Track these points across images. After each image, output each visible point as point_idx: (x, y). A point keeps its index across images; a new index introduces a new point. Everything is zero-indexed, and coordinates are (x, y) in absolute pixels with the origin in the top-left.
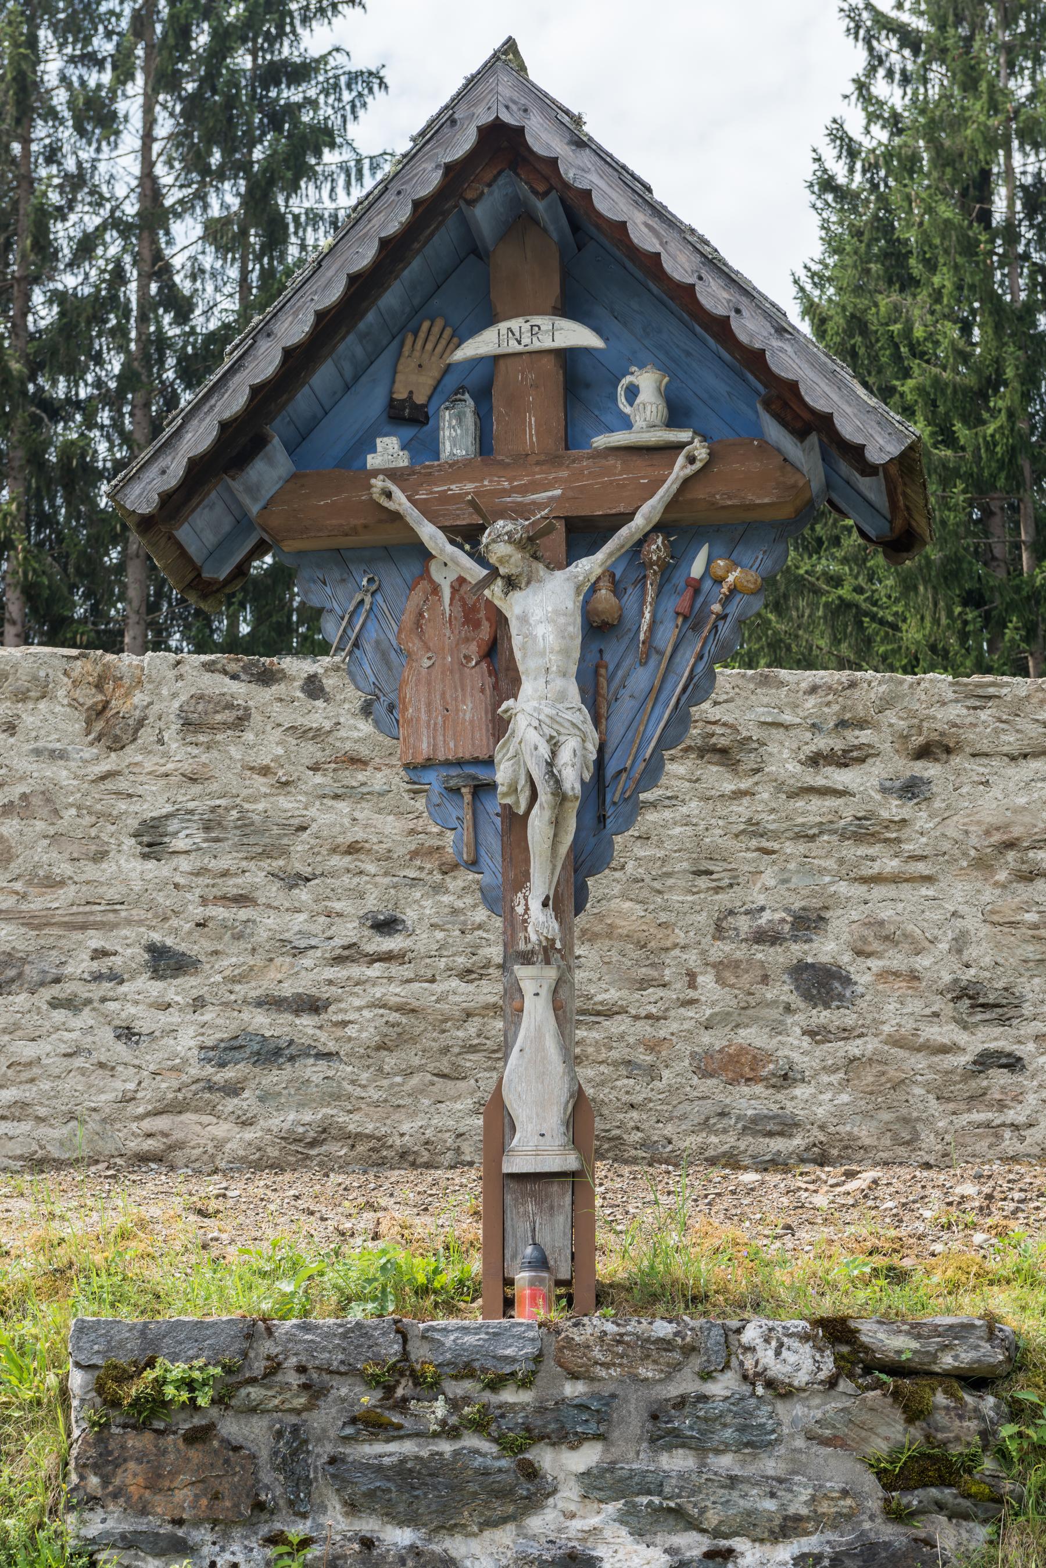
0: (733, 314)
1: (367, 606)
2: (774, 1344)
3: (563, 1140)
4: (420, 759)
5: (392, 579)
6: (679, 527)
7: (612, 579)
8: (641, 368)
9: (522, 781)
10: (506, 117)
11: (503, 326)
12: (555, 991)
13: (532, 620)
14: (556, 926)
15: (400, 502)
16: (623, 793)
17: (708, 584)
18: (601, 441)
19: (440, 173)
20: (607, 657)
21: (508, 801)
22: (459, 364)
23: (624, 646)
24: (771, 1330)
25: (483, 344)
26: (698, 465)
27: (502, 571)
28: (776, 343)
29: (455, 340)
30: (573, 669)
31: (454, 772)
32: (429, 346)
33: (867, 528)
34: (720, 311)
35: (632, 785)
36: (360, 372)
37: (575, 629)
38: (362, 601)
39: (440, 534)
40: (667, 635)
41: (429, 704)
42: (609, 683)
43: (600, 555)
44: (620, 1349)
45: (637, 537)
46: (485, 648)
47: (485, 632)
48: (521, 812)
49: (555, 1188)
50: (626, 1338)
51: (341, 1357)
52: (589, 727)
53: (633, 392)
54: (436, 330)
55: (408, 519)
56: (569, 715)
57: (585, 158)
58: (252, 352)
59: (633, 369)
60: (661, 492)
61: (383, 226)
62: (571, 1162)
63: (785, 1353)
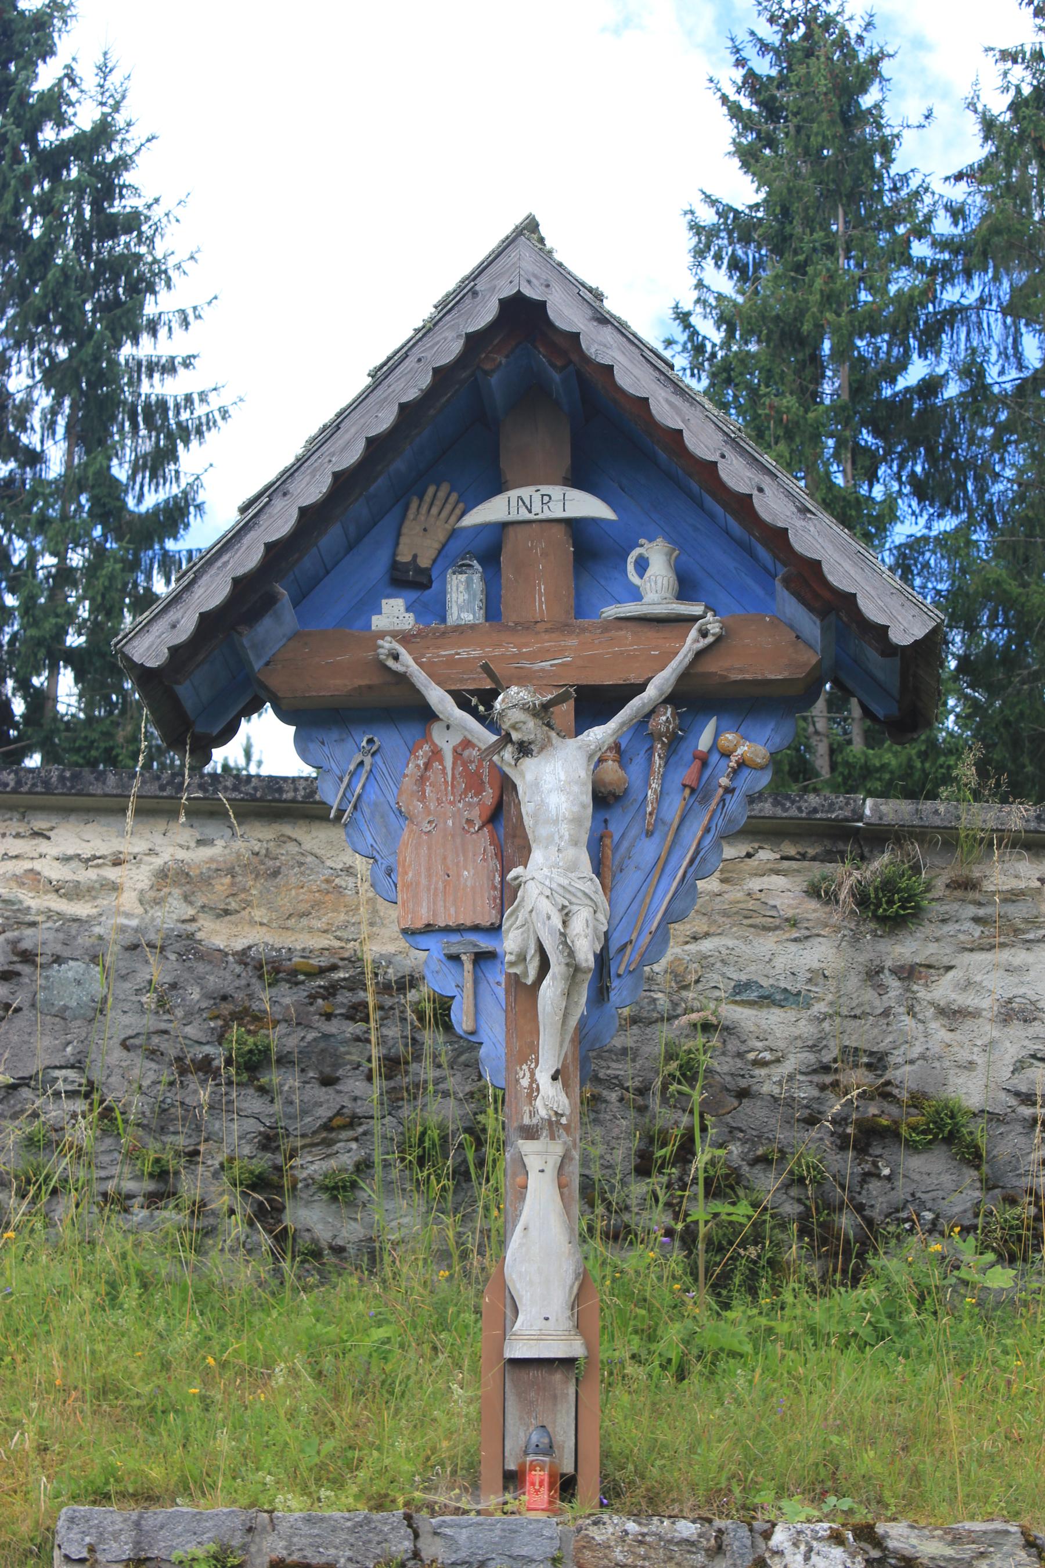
0: (755, 492)
1: (367, 767)
2: (803, 1548)
3: (569, 1324)
4: (419, 924)
5: (390, 739)
6: (693, 698)
7: (618, 751)
8: (651, 540)
9: (532, 950)
10: (528, 292)
11: (513, 494)
12: (561, 1168)
13: (546, 787)
14: (566, 1101)
15: (407, 663)
16: (628, 965)
17: (715, 758)
18: (611, 611)
19: (461, 342)
20: (612, 827)
21: (517, 970)
22: (465, 528)
23: (628, 818)
24: (799, 1532)
25: (493, 510)
26: (710, 639)
27: (515, 736)
28: (799, 523)
29: (461, 506)
30: (585, 837)
31: (455, 938)
32: (434, 511)
33: (874, 708)
34: (742, 488)
35: (636, 957)
36: (364, 531)
37: (588, 799)
38: (362, 763)
39: (449, 699)
40: (674, 806)
41: (429, 869)
42: (613, 854)
43: (613, 724)
44: (642, 1551)
45: (647, 710)
46: (488, 813)
47: (489, 796)
48: (529, 981)
49: (558, 1377)
50: (648, 1539)
51: (348, 1553)
52: (601, 898)
53: (642, 566)
54: (442, 494)
55: (415, 680)
56: (579, 885)
57: (607, 333)
58: (268, 510)
59: (642, 541)
60: (674, 664)
61: (404, 391)
62: (575, 1348)
63: (814, 1558)
